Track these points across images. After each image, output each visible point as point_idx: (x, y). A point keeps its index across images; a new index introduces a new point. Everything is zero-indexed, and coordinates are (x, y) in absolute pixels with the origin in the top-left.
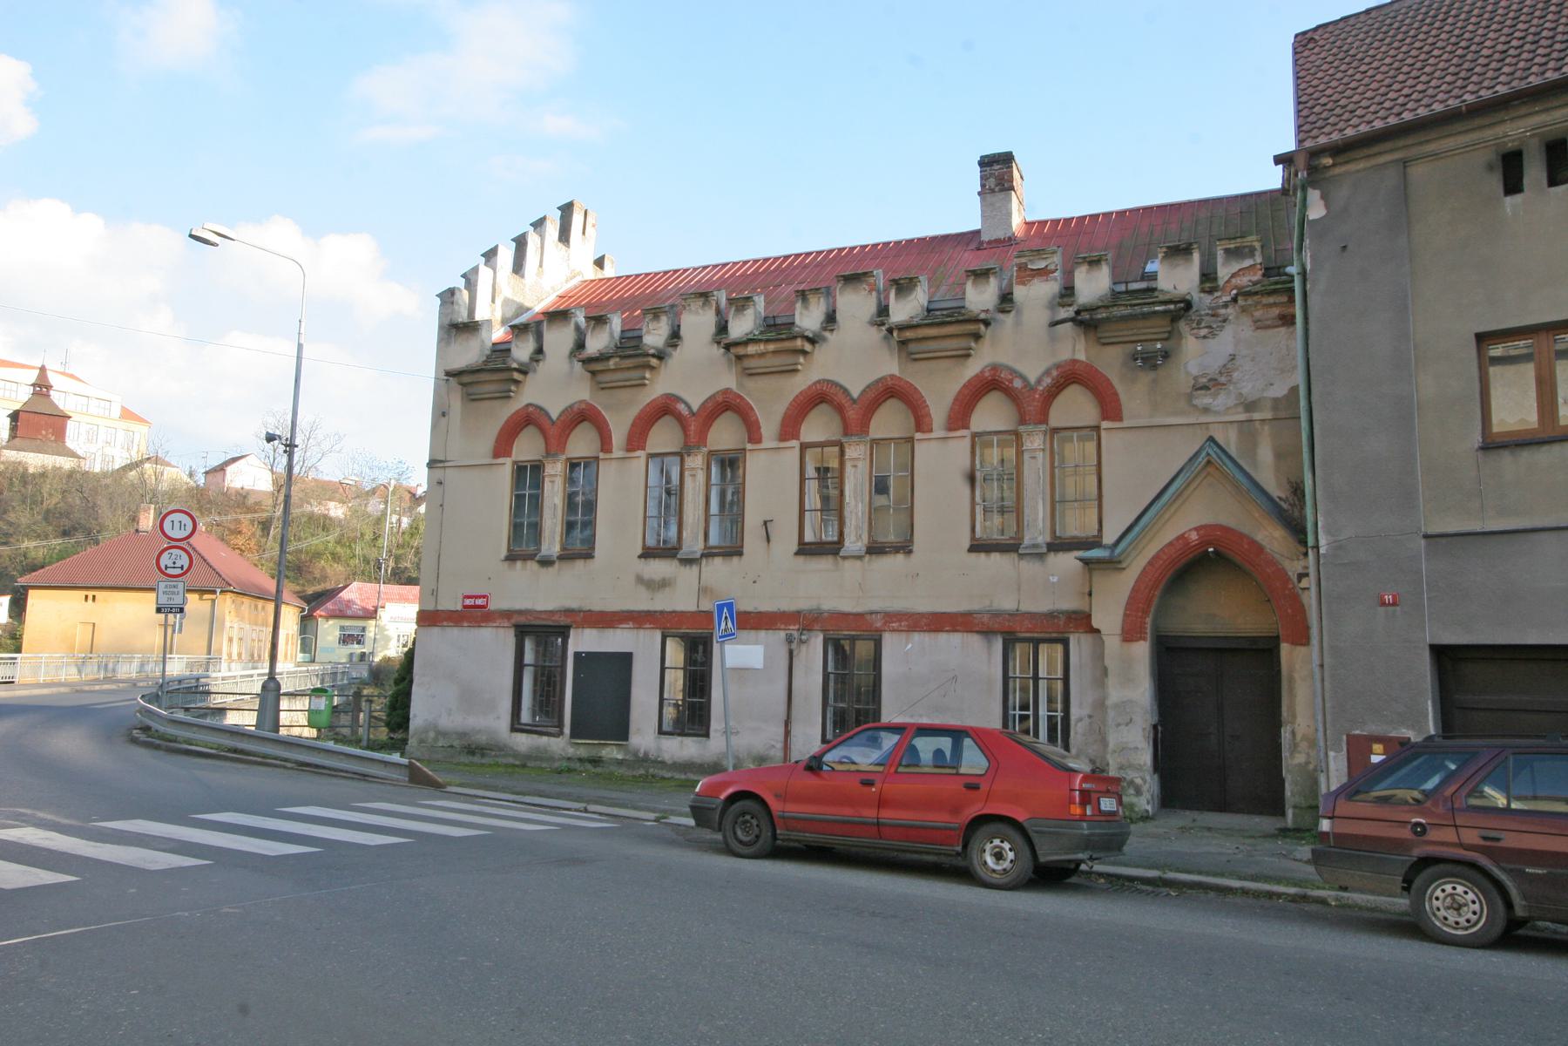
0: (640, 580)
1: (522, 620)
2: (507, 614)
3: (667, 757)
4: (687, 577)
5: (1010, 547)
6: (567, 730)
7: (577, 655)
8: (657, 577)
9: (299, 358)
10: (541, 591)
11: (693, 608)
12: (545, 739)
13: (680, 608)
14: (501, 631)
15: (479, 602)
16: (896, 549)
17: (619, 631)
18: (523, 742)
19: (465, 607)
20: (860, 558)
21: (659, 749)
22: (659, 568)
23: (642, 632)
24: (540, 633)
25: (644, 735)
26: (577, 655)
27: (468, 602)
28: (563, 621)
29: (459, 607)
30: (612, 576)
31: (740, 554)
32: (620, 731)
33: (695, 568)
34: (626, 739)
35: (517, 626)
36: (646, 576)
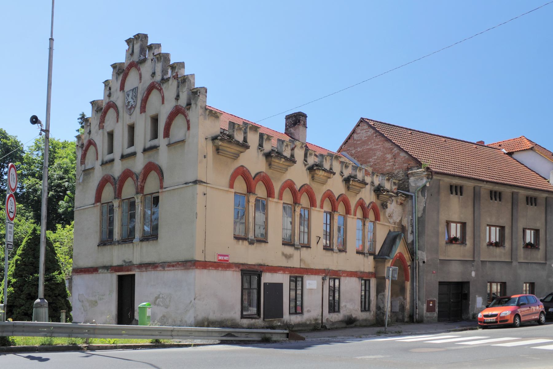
0: (283, 254)
1: (244, 268)
2: (237, 265)
3: (292, 323)
4: (296, 254)
5: (245, 239)
6: (262, 316)
7: (264, 284)
8: (288, 254)
9: (51, 49)
10: (251, 255)
11: (299, 267)
12: (254, 320)
13: (295, 266)
14: (235, 273)
15: (226, 258)
16: (260, 241)
17: (278, 274)
18: (246, 322)
19: (219, 260)
20: (538, 322)
21: (290, 320)
22: (289, 250)
23: (285, 275)
24: (250, 274)
25: (286, 317)
26: (264, 284)
27: (220, 258)
28: (259, 269)
29: (216, 260)
30: (271, 253)
31: (266, 242)
32: (280, 315)
33: (299, 251)
34: (282, 317)
35: (242, 270)
36: (285, 253)
